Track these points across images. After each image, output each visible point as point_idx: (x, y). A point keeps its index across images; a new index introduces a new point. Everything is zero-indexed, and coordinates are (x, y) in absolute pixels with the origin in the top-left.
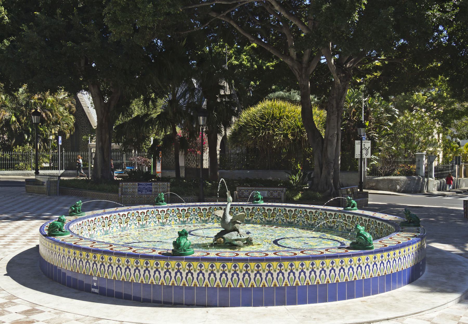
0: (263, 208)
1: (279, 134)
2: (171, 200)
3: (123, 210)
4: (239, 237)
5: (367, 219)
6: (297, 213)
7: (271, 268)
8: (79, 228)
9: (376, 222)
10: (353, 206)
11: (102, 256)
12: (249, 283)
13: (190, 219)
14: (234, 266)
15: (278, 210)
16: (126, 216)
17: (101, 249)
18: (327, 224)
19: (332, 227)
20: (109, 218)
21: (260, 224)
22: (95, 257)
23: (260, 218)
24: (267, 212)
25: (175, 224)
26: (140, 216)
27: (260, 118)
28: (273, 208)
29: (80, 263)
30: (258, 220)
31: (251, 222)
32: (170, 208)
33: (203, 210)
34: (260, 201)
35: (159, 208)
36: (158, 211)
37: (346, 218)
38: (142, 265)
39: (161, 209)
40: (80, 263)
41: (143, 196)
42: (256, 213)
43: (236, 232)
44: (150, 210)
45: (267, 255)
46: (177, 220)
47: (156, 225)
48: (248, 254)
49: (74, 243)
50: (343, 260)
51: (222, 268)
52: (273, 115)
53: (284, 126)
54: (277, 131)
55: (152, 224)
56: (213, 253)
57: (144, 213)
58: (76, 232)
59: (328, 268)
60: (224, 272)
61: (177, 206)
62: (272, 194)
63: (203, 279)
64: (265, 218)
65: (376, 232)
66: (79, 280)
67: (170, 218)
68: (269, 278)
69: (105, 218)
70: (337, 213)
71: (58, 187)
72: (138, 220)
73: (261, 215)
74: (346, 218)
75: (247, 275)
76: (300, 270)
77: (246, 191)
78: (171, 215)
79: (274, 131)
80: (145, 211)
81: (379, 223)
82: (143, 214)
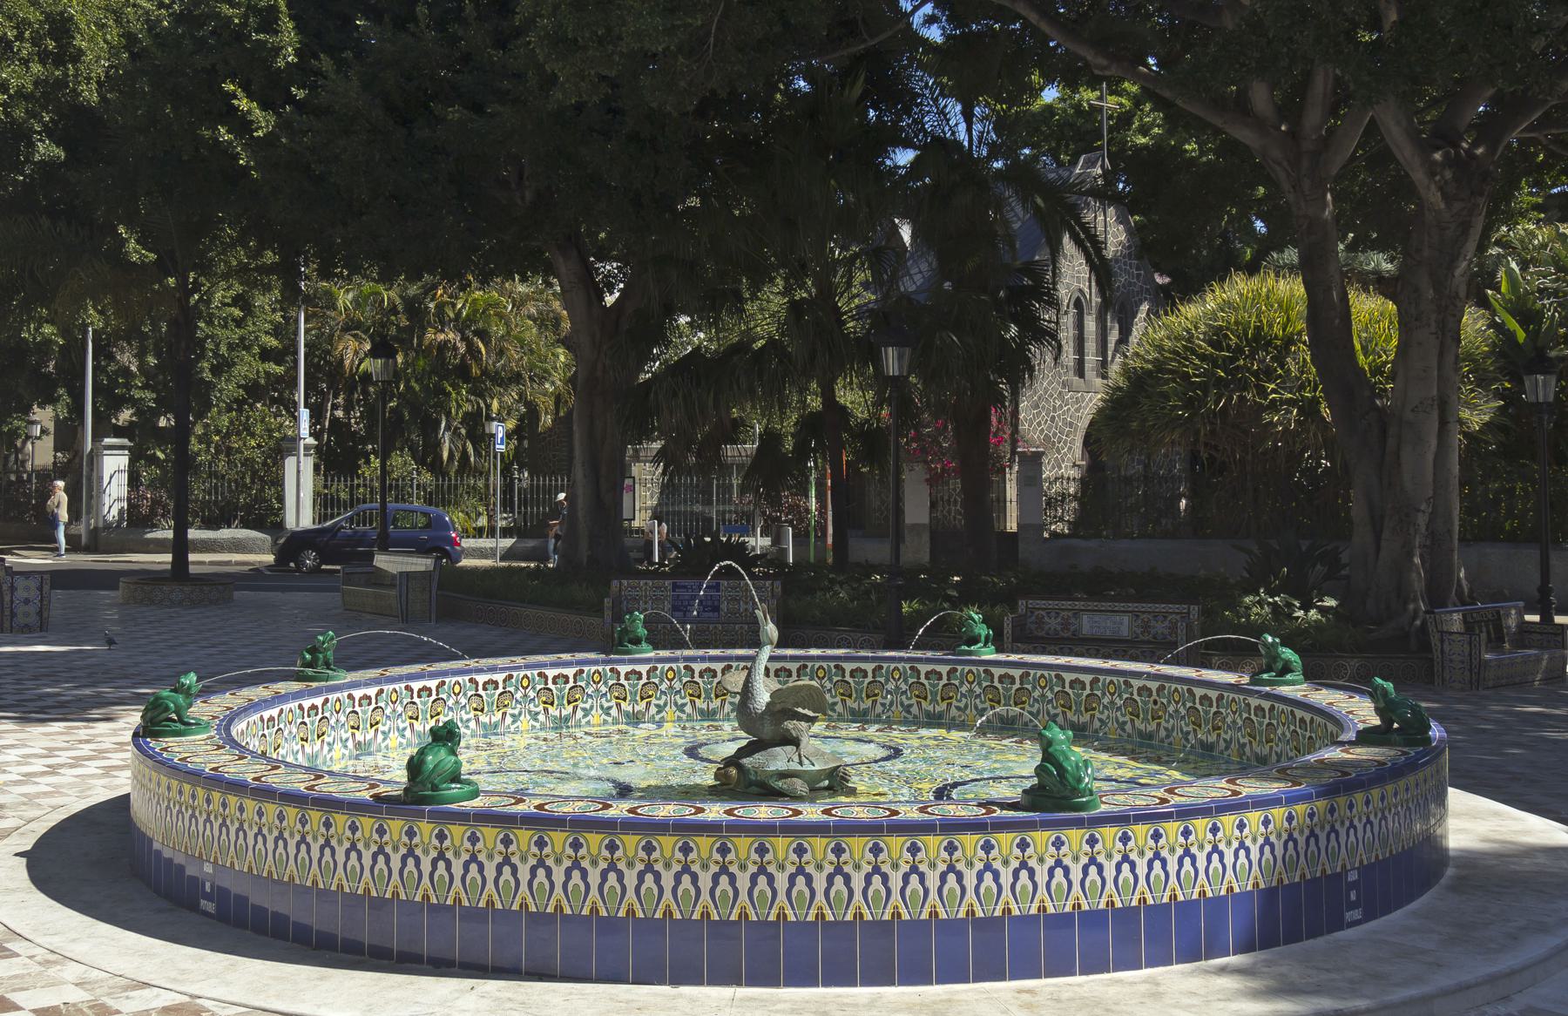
0: (985, 671)
1: (1283, 402)
2: (663, 637)
3: (559, 668)
4: (795, 766)
5: (1214, 694)
6: (1029, 687)
7: (807, 857)
8: (266, 732)
9: (1294, 716)
10: (1287, 669)
11: (327, 819)
12: (620, 903)
13: (657, 706)
14: (681, 849)
15: (1036, 681)
16: (434, 692)
17: (341, 796)
18: (1133, 726)
19: (1150, 736)
20: (374, 701)
21: (905, 722)
22: (328, 825)
23: (902, 704)
24: (850, 680)
25: (679, 719)
26: (480, 696)
27: (1211, 343)
28: (1020, 672)
29: (237, 837)
30: (897, 710)
31: (871, 717)
32: (660, 666)
33: (555, 679)
34: (980, 645)
35: (622, 662)
36: (477, 683)
37: (1197, 701)
38: (457, 843)
39: (629, 668)
40: (237, 837)
41: (711, 627)
42: (964, 689)
43: (790, 749)
44: (515, 674)
45: (896, 813)
46: (610, 708)
47: (610, 719)
48: (833, 812)
49: (254, 779)
50: (1161, 831)
51: (717, 857)
52: (1258, 329)
53: (1302, 373)
54: (1274, 391)
55: (596, 717)
56: (714, 812)
57: (496, 683)
58: (255, 744)
59: (1109, 856)
60: (686, 869)
61: (687, 659)
62: (1146, 627)
63: (583, 888)
64: (919, 704)
65: (1191, 726)
66: (235, 895)
67: (659, 699)
68: (686, 890)
69: (361, 699)
70: (810, 665)
71: (434, 592)
72: (545, 703)
73: (905, 692)
74: (1197, 701)
75: (612, 876)
76: (979, 866)
77: (1053, 614)
78: (519, 695)
79: (1263, 392)
80: (499, 677)
81: (1204, 698)
82: (560, 681)
